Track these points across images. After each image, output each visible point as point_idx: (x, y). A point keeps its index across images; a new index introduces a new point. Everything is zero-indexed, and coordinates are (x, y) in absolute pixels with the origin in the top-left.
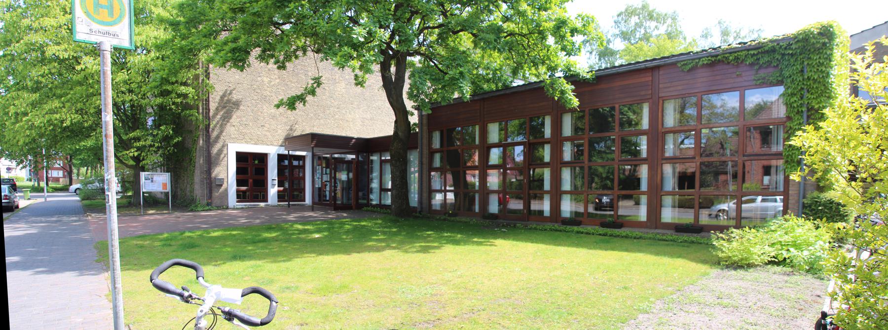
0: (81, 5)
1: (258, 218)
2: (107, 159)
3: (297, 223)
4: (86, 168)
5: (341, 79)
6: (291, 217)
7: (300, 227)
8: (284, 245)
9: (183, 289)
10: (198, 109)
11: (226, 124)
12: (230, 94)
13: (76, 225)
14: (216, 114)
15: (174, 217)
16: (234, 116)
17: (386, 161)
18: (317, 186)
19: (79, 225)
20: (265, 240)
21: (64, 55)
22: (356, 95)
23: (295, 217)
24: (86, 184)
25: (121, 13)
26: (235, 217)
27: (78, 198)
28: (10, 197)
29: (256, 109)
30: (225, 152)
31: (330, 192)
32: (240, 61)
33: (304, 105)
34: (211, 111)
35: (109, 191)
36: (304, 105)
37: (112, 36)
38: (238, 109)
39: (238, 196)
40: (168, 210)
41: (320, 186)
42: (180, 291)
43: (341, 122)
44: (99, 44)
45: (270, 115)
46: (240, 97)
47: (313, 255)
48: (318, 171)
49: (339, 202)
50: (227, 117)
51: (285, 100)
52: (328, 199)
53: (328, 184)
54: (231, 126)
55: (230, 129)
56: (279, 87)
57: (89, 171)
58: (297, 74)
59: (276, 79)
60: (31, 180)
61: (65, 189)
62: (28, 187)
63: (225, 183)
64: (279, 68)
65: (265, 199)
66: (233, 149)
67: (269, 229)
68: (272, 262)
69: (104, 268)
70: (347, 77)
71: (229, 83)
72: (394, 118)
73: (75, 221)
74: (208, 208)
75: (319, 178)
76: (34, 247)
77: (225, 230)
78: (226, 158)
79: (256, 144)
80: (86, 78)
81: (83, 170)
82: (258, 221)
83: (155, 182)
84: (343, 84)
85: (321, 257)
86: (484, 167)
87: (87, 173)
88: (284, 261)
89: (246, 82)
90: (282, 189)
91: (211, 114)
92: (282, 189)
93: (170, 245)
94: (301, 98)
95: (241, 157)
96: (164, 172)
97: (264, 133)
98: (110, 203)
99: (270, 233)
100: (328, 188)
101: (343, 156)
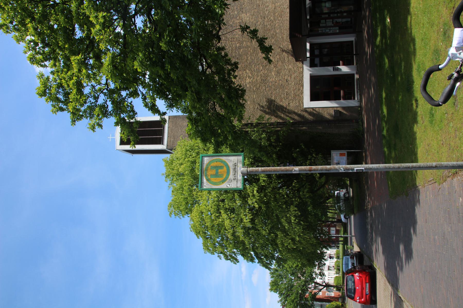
0: (218, 185)
1: (370, 79)
2: (328, 170)
3: (375, 43)
4: (328, 213)
5: (238, 18)
6: (368, 50)
7: (379, 39)
8: (397, 49)
9: (450, 78)
10: (278, 131)
11: (288, 110)
12: (262, 107)
13: (375, 215)
14: (281, 118)
15: (369, 147)
16: (281, 103)
18: (338, 31)
19: (375, 212)
20: (392, 67)
21: (249, 216)
22: (251, 2)
23: (369, 47)
24: (341, 211)
25: (219, 162)
26: (369, 100)
27: (352, 217)
28: (352, 256)
29: (273, 87)
30: (311, 110)
31: (343, 17)
32: (237, 92)
33: (266, 39)
34: (278, 121)
35: (354, 169)
36: (266, 39)
37: (236, 167)
38: (274, 101)
39: (350, 99)
40: (362, 153)
41: (338, 28)
42: (452, 81)
43: (277, 14)
44: (243, 175)
45: (277, 75)
46: (265, 99)
47: (409, 19)
48: (324, 31)
49: (352, 7)
50: (282, 109)
51: (264, 55)
52: (349, 20)
53: (335, 20)
54: (289, 106)
55: (292, 106)
56: (253, 70)
57: (330, 211)
58: (240, 56)
59: (246, 72)
60: (339, 247)
61: (345, 226)
62: (344, 248)
63: (338, 109)
64: (237, 68)
65: (351, 76)
67: (381, 65)
68: (415, 55)
69: (413, 190)
70: (236, 13)
71: (254, 109)
73: (371, 215)
74: (360, 122)
75: (330, 30)
76: (393, 238)
77: (385, 99)
78: (316, 109)
79: (303, 86)
80: (263, 202)
81: (329, 215)
82: (373, 79)
83: (339, 161)
84: (243, 15)
85: (411, 10)
87: (332, 213)
88: (414, 45)
89: (252, 96)
90: (341, 62)
91: (281, 121)
92: (341, 62)
93: (395, 145)
94: (261, 42)
95: (313, 98)
96: (331, 157)
97: (292, 79)
98: (363, 168)
99: (385, 64)
100: (339, 20)
101: (308, 10)
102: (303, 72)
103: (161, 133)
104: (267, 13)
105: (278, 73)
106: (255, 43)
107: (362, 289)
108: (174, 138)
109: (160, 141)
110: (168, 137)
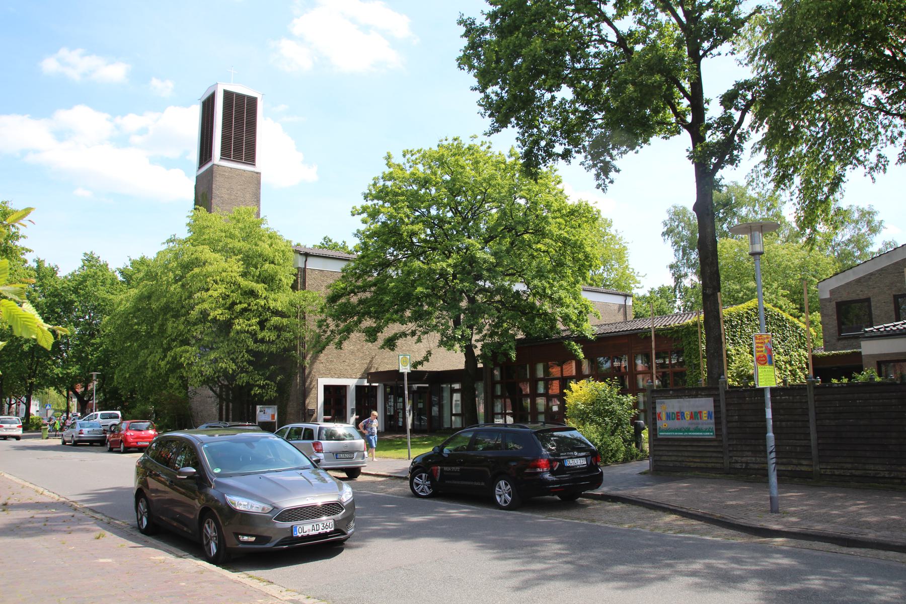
17: (456, 391)
41: (392, 413)
55: (318, 366)
66: (323, 381)
72: (464, 359)
86: (534, 395)
95: (327, 388)
97: (345, 367)
102: (351, 378)
103: (238, 159)
104: (410, 343)
105: (352, 353)
106: (419, 359)
107: (143, 438)
108: (228, 178)
109: (225, 155)
110: (231, 168)
